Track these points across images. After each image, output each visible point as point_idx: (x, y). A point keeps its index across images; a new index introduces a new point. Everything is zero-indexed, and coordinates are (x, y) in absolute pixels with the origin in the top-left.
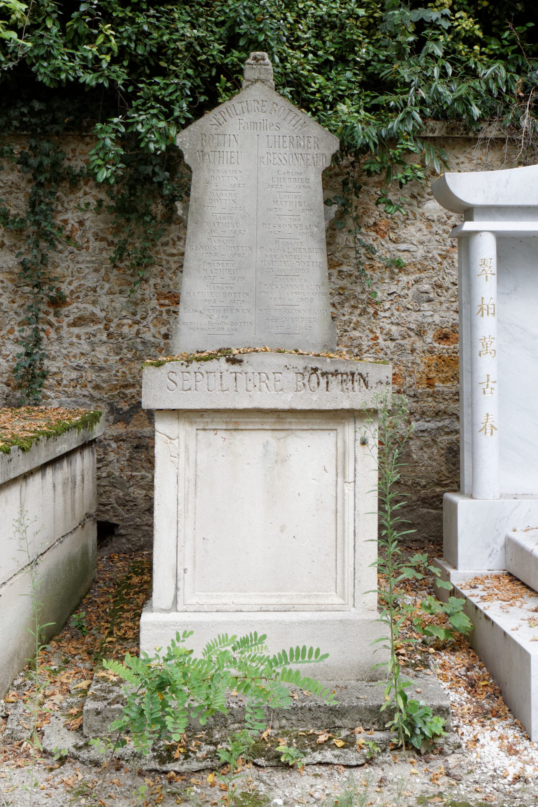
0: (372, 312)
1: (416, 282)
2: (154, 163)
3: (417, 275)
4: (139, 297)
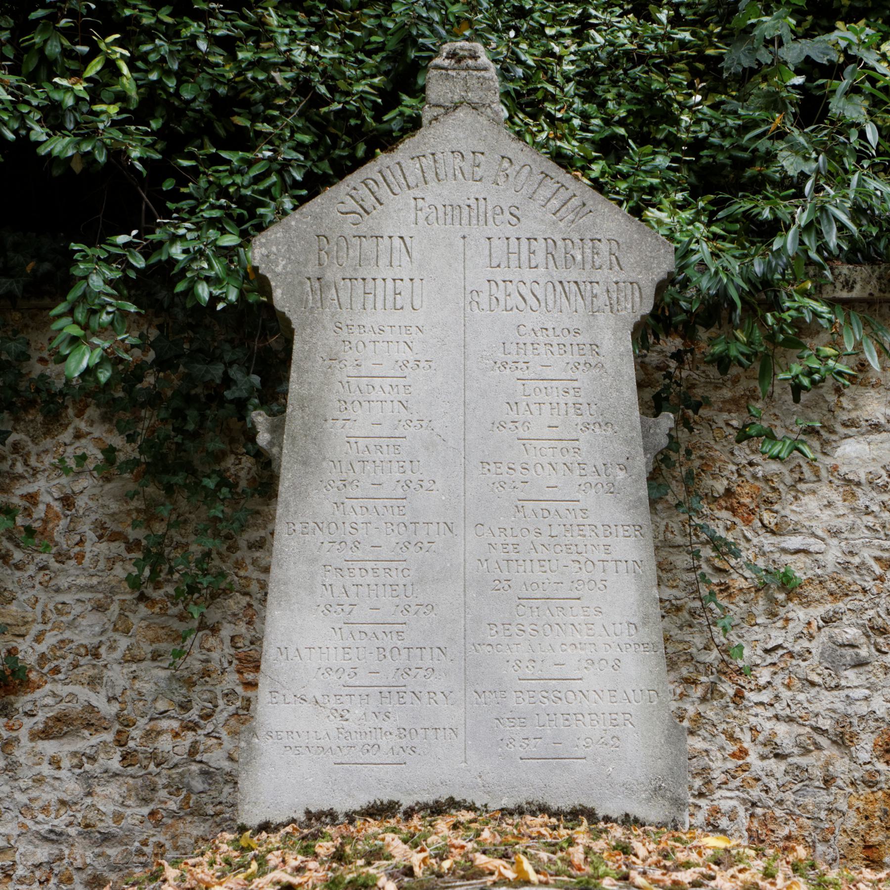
0: (731, 692)
1: (827, 621)
2: (227, 357)
3: (829, 606)
4: (198, 666)
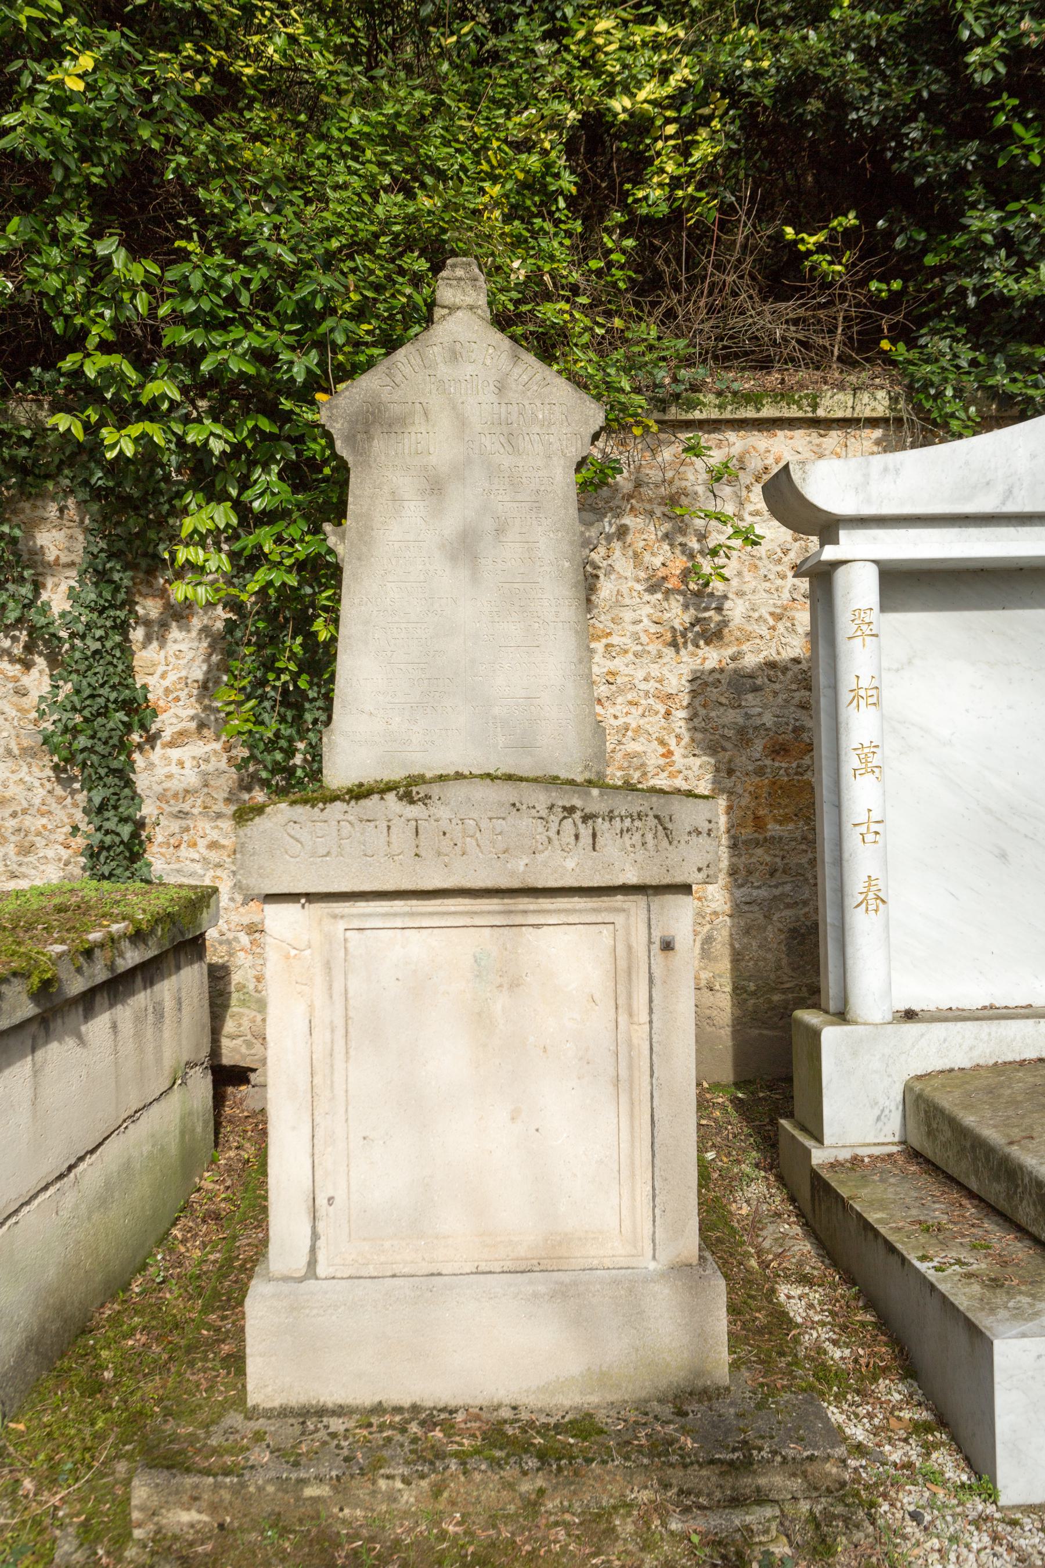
3: (735, 649)
